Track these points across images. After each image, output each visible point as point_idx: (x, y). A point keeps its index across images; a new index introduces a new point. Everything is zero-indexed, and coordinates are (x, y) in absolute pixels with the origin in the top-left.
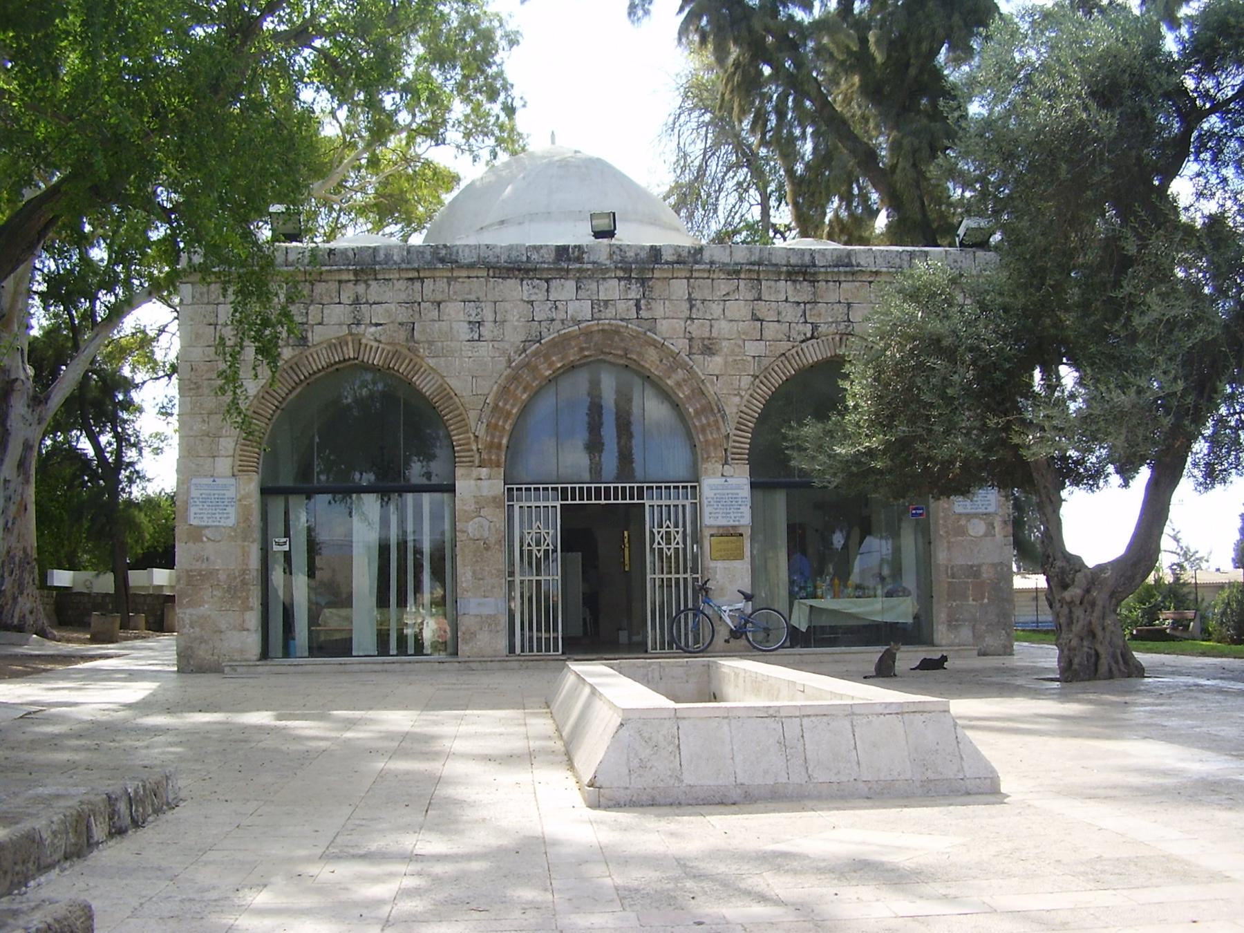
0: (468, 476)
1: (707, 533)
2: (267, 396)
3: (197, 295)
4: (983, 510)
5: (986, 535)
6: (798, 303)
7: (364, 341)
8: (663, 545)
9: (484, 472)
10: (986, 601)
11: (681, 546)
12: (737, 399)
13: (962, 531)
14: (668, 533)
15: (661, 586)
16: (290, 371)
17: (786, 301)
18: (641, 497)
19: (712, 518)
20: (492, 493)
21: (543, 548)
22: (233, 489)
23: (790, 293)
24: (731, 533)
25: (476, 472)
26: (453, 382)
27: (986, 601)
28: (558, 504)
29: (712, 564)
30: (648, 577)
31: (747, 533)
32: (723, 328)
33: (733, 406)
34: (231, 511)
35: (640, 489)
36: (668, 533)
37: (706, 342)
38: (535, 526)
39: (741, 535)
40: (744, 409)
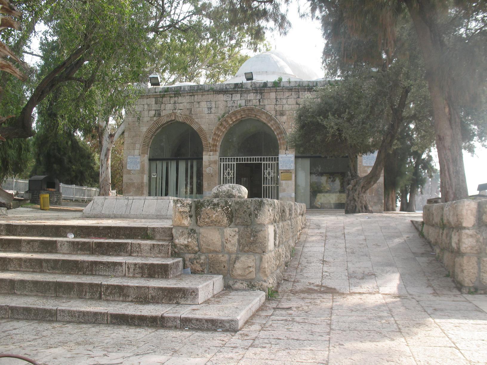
21: (230, 176)
24: (288, 171)
25: (209, 153)
28: (235, 163)
29: (281, 182)
34: (139, 165)
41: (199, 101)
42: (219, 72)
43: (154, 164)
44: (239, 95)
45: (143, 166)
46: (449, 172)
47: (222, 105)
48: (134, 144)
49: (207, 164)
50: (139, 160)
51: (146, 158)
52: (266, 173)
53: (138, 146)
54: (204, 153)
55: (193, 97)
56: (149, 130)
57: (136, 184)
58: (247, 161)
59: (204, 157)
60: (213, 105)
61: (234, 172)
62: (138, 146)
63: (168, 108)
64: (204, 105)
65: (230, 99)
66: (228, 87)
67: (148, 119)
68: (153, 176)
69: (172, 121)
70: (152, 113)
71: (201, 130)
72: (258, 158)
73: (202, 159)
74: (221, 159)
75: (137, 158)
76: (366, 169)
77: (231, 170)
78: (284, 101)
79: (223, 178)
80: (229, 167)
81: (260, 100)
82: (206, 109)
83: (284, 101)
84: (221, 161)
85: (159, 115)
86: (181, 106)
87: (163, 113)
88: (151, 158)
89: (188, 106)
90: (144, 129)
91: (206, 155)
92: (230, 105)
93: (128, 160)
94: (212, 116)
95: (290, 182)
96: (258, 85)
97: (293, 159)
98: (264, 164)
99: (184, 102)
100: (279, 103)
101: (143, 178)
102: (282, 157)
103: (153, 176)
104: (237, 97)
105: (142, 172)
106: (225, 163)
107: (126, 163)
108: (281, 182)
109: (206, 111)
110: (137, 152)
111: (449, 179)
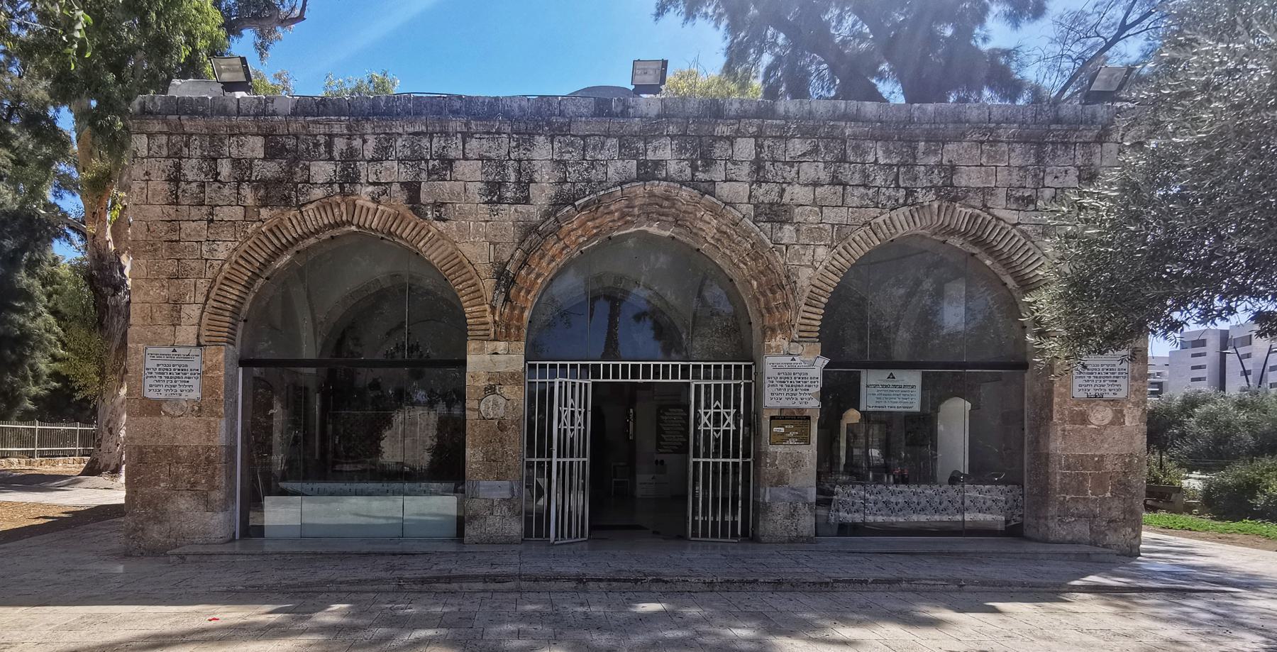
0: (482, 350)
1: (766, 416)
2: (242, 262)
3: (155, 148)
4: (1111, 396)
5: (1112, 423)
6: (891, 166)
7: (359, 202)
8: (711, 427)
9: (501, 346)
10: (1108, 494)
11: (732, 427)
12: (810, 271)
13: (1083, 419)
14: (717, 415)
15: (716, 473)
16: (270, 235)
17: (876, 162)
18: (685, 376)
19: (773, 399)
20: (511, 370)
21: (723, 428)
22: (197, 359)
23: (880, 153)
24: (797, 419)
25: (490, 346)
26: (467, 249)
27: (1108, 494)
28: (590, 381)
29: (772, 449)
30: (692, 460)
31: (816, 417)
32: (798, 193)
33: (805, 277)
34: (195, 383)
35: (685, 368)
36: (717, 415)
37: (775, 208)
38: (576, 432)
39: (808, 418)
40: (817, 283)
46: (738, 411)
52: (704, 419)
53: (191, 312)
54: (472, 345)
58: (635, 375)
59: (470, 359)
62: (191, 312)
69: (337, 225)
72: (606, 367)
74: (532, 367)
93: (150, 364)
98: (698, 387)
102: (774, 366)
110: (187, 333)
111: (167, 621)
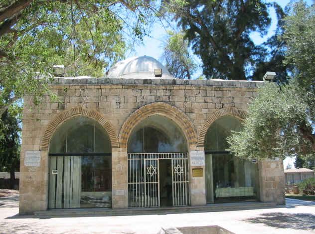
29: (193, 178)
34: (39, 162)
41: (107, 95)
42: (240, 47)
43: (54, 159)
44: (148, 91)
45: (43, 162)
47: (131, 100)
48: (33, 138)
49: (117, 161)
50: (38, 156)
51: (46, 154)
55: (100, 90)
56: (52, 124)
57: (35, 183)
59: (113, 154)
60: (122, 100)
61: (184, 168)
62: (38, 140)
63: (72, 103)
64: (112, 99)
65: (139, 94)
66: (137, 82)
67: (51, 111)
68: (53, 173)
70: (55, 105)
71: (108, 125)
73: (110, 154)
75: (36, 154)
76: (269, 164)
77: (181, 166)
78: (193, 99)
79: (147, 174)
80: (179, 164)
81: (169, 96)
82: (115, 104)
83: (193, 99)
84: (129, 158)
85: (63, 108)
86: (88, 99)
87: (67, 106)
88: (51, 153)
89: (95, 100)
90: (45, 122)
91: (114, 151)
92: (139, 101)
93: (27, 156)
94: (121, 111)
95: (201, 178)
96: (167, 82)
97: (203, 155)
99: (91, 95)
100: (188, 101)
101: (43, 175)
103: (53, 173)
104: (146, 93)
105: (42, 169)
106: (148, 159)
107: (24, 159)
108: (193, 178)
109: (114, 105)
110: (37, 147)
